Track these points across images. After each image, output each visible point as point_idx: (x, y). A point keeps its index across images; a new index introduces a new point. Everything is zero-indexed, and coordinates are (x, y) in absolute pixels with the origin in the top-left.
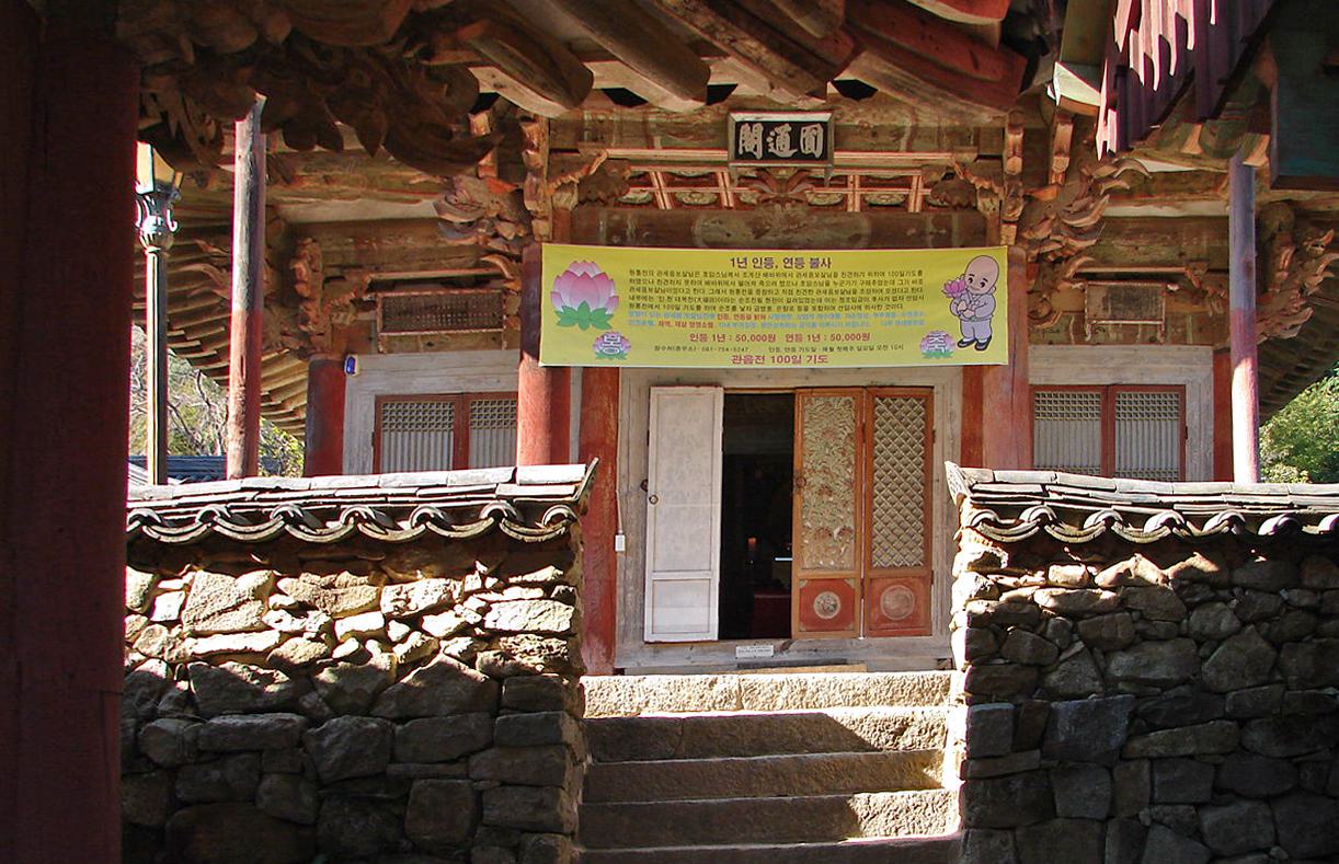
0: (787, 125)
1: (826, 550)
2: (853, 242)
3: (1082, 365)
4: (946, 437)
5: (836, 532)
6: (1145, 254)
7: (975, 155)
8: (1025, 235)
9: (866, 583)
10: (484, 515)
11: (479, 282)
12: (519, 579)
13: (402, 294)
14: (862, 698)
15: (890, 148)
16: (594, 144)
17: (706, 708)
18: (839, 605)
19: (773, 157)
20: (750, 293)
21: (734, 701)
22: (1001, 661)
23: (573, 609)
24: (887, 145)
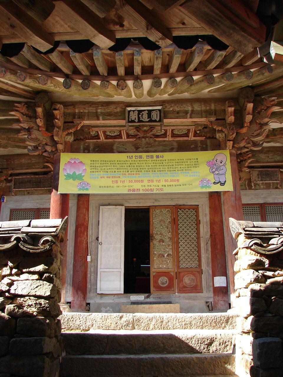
0: (146, 111)
1: (162, 262)
2: (171, 150)
4: (204, 223)
5: (166, 255)
6: (272, 159)
7: (215, 118)
8: (236, 145)
9: (178, 273)
10: (12, 239)
11: (45, 173)
12: (28, 270)
13: (20, 177)
14: (188, 325)
15: (184, 117)
16: (79, 119)
17: (119, 328)
18: (168, 282)
19: (142, 121)
20: (134, 166)
21: (131, 325)
22: (270, 315)
23: (52, 285)
24: (183, 116)
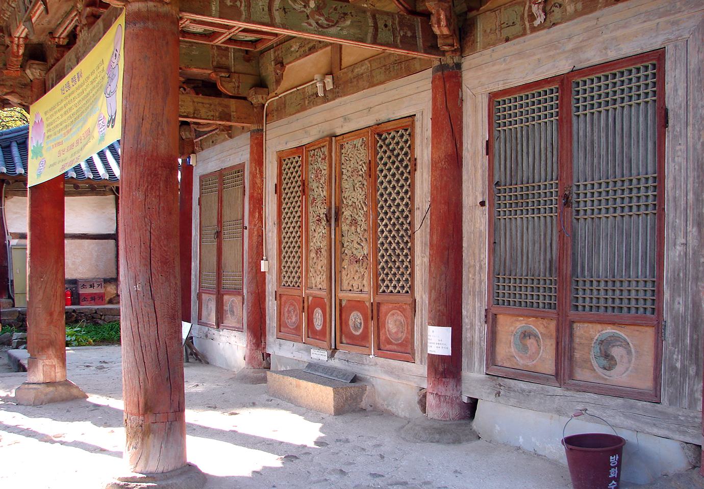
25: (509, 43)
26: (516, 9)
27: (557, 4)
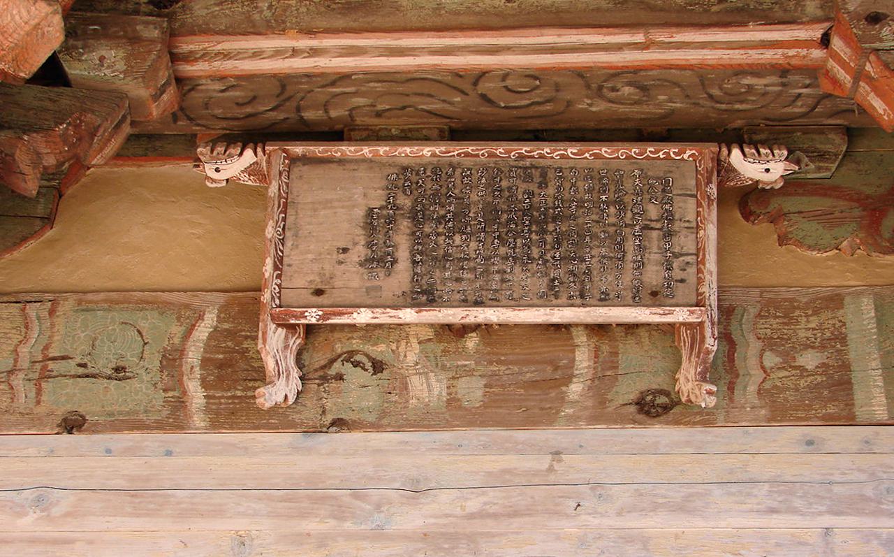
3: (241, 525)
25: (76, 438)
26: (144, 325)
27: (358, 358)
